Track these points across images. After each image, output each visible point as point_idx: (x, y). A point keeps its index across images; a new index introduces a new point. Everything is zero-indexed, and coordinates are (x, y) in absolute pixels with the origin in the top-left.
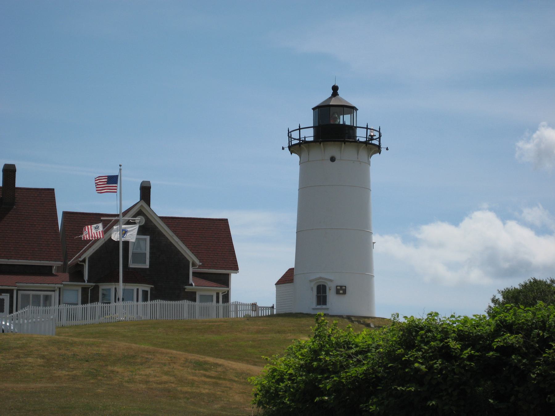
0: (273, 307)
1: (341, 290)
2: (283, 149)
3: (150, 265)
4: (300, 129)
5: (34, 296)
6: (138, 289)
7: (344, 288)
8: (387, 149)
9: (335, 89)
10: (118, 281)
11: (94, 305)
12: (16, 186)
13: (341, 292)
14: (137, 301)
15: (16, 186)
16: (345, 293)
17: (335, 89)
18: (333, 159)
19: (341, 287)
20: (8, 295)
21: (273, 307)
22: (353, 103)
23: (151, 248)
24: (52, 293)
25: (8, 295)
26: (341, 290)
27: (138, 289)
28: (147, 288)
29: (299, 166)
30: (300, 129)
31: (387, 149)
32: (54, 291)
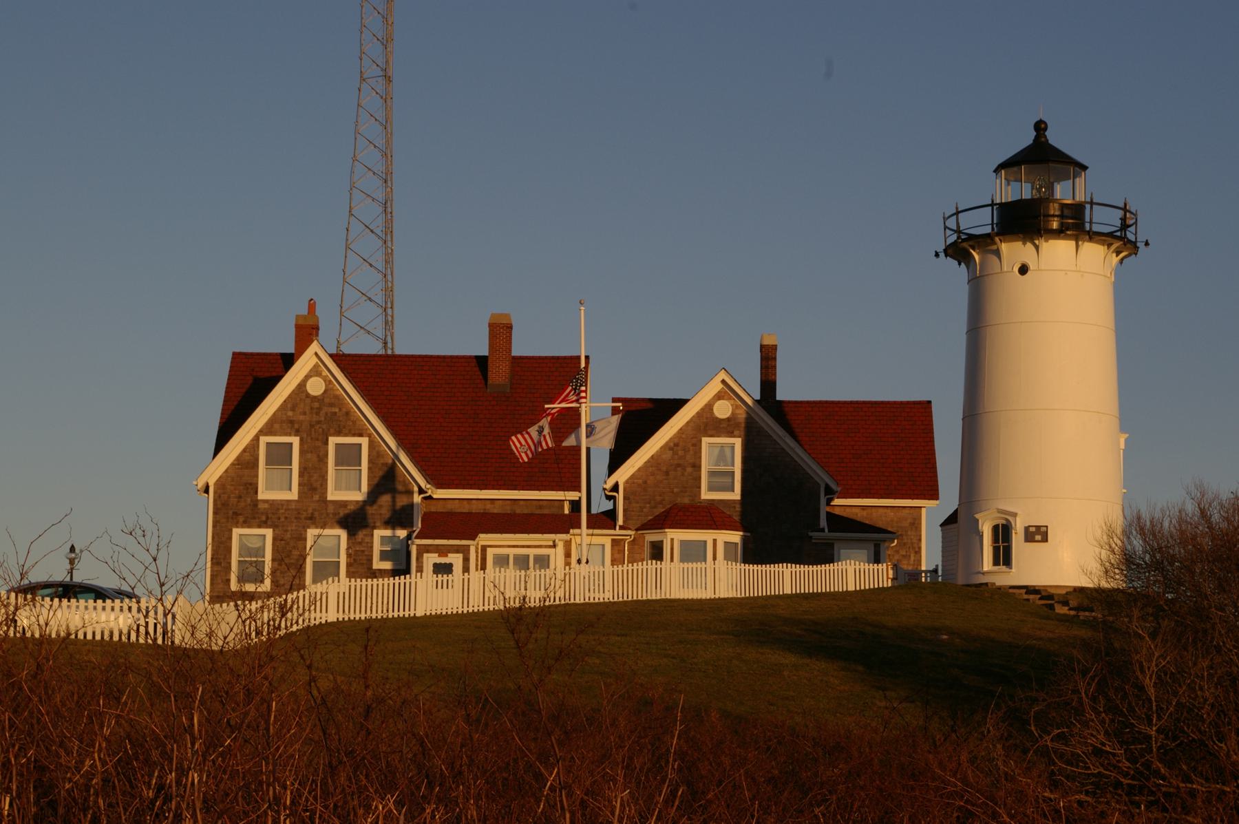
0: (936, 571)
1: (1037, 534)
2: (937, 255)
3: (743, 495)
5: (516, 558)
6: (715, 541)
7: (1043, 529)
8: (1147, 244)
10: (579, 527)
11: (640, 567)
12: (778, 398)
13: (1038, 537)
14: (672, 560)
15: (778, 398)
16: (1045, 539)
19: (1038, 527)
20: (461, 556)
21: (936, 571)
22: (1085, 163)
23: (745, 460)
24: (490, 553)
25: (461, 556)
26: (1037, 534)
27: (715, 541)
28: (735, 537)
29: (967, 287)
30: (957, 213)
31: (1147, 244)
32: (554, 546)
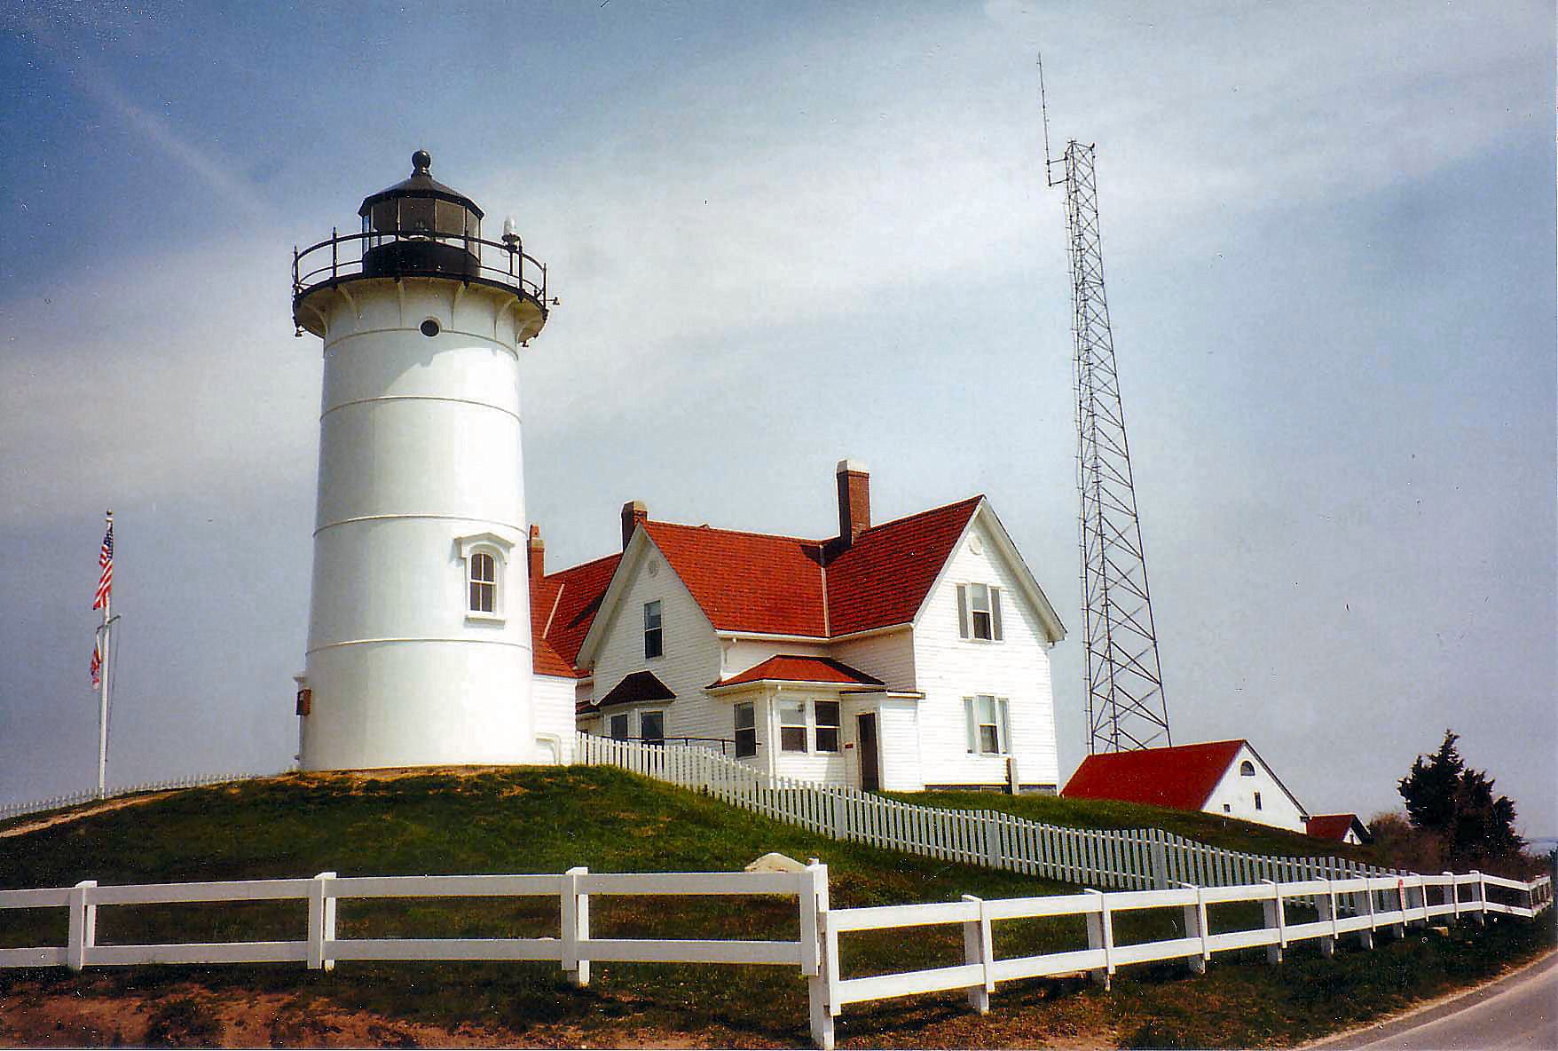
9: (421, 160)
17: (421, 160)
30: (335, 241)
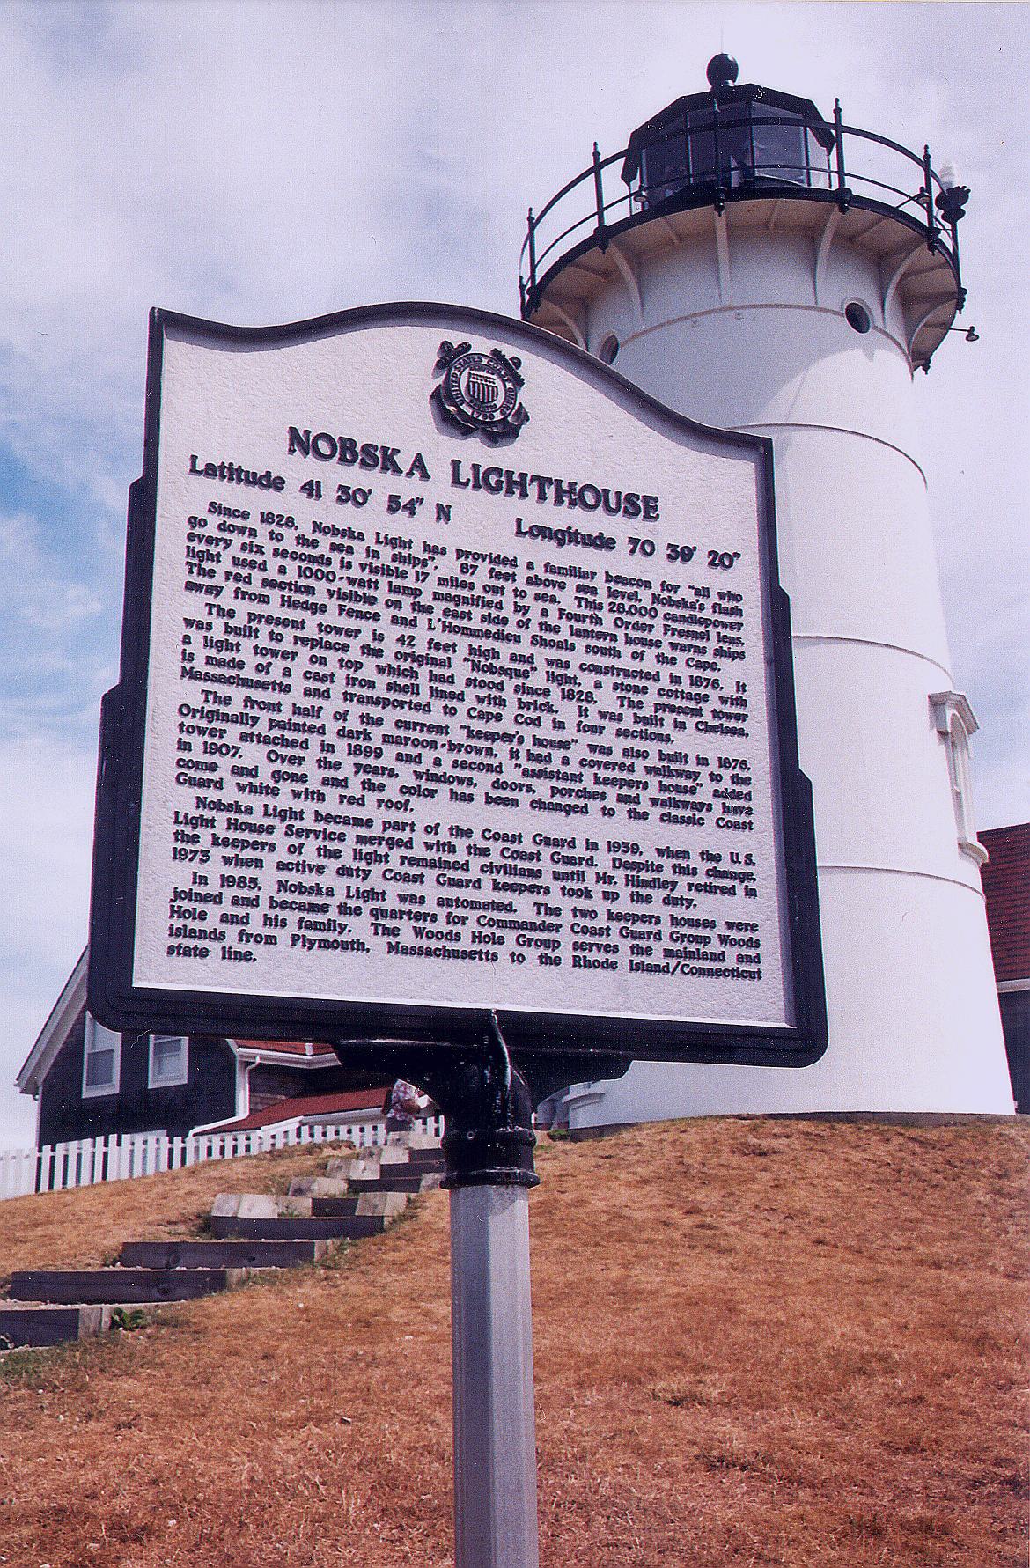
4: (597, 167)
8: (971, 335)
18: (857, 318)
30: (597, 167)
